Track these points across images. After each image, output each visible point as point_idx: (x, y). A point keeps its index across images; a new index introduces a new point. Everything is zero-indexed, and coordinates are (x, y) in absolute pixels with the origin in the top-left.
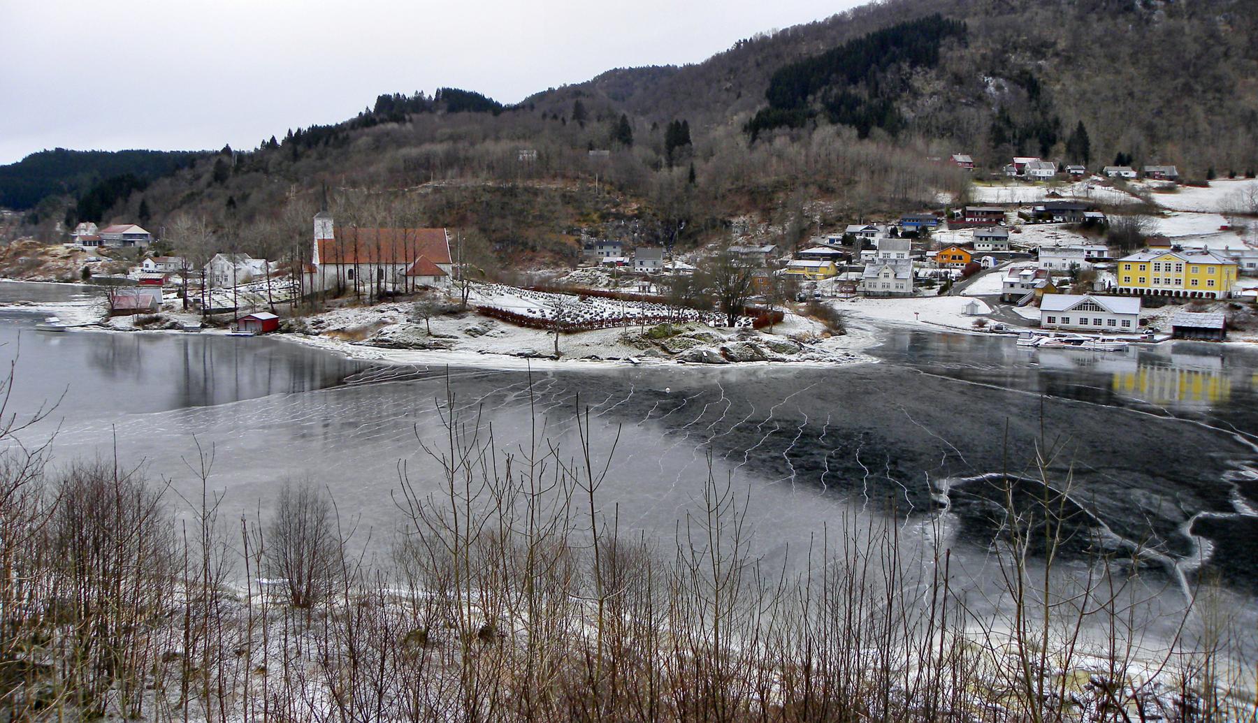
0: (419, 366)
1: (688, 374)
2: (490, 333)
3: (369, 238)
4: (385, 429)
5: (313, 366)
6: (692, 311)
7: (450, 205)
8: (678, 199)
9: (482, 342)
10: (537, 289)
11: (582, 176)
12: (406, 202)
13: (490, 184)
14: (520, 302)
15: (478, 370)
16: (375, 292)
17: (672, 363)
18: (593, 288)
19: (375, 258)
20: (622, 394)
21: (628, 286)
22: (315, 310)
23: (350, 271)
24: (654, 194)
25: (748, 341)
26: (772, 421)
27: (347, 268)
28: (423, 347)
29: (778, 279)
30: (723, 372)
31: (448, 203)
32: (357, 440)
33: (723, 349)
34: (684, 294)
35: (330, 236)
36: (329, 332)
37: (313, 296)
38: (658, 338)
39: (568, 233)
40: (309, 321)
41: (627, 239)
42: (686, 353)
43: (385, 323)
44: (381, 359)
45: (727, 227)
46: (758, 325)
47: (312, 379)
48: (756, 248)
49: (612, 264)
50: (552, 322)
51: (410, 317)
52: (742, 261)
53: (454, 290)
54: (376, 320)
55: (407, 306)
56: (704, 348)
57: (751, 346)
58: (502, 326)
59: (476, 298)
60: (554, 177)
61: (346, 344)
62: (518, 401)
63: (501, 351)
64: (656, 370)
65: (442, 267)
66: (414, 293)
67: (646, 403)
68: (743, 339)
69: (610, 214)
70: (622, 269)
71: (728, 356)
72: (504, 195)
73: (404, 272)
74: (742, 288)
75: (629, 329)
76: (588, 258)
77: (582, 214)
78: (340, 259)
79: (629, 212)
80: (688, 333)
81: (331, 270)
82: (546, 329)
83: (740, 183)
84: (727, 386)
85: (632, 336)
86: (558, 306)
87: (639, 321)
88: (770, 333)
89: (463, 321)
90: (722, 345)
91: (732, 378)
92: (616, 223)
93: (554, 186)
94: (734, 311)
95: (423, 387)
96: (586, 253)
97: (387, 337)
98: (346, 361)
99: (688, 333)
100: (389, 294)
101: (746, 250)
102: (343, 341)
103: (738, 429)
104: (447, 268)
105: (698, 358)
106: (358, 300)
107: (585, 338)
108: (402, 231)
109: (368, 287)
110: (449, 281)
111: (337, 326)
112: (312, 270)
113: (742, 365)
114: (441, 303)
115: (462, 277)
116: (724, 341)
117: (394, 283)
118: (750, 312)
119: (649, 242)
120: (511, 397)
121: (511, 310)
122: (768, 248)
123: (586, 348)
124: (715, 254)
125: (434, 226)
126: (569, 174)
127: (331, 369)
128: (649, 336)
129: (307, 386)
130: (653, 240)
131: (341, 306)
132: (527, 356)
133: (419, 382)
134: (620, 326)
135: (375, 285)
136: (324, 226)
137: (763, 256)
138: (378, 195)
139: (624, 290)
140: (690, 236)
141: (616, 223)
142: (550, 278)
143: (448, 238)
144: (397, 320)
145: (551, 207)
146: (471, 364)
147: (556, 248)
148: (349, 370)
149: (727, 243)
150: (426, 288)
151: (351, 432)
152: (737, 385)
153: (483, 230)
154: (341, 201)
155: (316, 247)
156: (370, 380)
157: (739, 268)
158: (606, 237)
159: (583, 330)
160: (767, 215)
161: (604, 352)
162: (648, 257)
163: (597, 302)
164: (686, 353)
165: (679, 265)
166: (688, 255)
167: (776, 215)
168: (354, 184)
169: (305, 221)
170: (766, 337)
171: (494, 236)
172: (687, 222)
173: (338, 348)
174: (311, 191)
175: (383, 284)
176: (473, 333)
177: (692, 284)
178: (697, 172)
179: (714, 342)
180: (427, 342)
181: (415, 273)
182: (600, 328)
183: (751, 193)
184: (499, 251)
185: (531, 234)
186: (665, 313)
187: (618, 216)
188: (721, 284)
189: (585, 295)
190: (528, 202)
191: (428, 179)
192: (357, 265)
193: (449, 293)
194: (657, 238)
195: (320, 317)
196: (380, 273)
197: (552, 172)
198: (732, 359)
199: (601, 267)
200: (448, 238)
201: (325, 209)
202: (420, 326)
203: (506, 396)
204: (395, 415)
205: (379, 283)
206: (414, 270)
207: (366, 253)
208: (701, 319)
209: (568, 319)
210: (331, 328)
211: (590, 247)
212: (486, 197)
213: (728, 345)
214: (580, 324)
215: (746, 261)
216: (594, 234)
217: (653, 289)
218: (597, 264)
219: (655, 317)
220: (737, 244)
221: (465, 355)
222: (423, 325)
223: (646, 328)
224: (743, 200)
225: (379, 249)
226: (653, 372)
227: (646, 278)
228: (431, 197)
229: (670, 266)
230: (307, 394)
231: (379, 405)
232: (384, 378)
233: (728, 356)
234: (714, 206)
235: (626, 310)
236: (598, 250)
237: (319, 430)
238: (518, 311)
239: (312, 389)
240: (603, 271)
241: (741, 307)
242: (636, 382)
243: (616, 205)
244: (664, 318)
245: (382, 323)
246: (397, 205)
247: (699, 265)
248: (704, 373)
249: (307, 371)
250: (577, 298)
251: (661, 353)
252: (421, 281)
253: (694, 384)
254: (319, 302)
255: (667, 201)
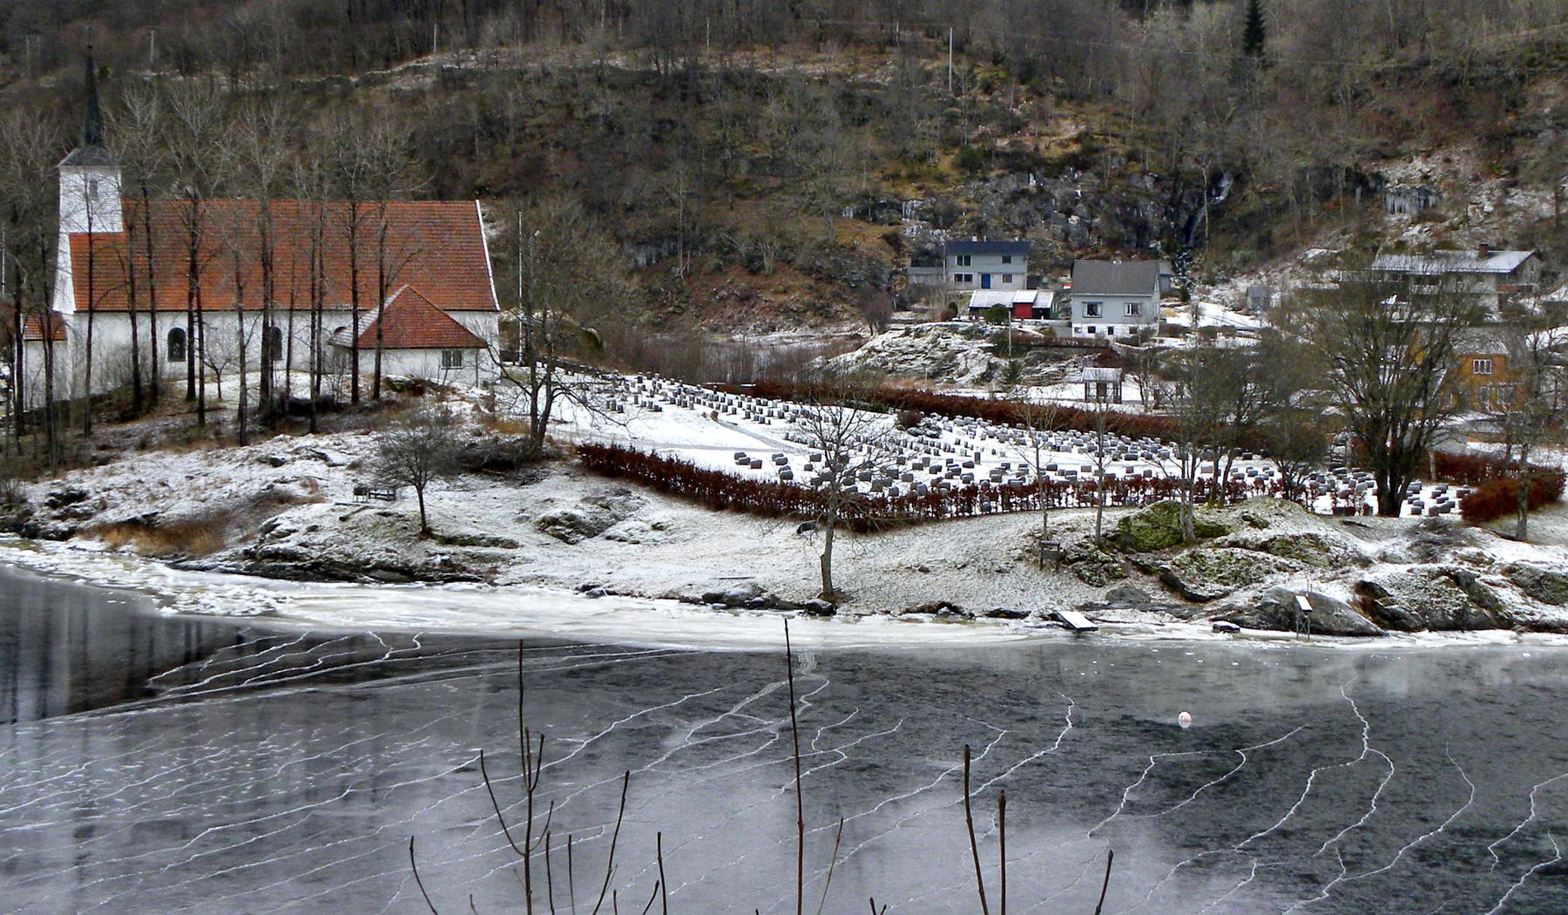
0: (391, 637)
1: (1248, 666)
2: (618, 529)
3: (236, 232)
4: (280, 842)
5: (47, 637)
6: (1258, 464)
7: (493, 128)
8: (1209, 107)
9: (592, 558)
10: (765, 391)
11: (906, 35)
12: (355, 120)
13: (619, 61)
14: (714, 433)
15: (579, 647)
16: (253, 401)
17: (1196, 631)
18: (940, 389)
19: (255, 293)
20: (1035, 730)
21: (1051, 380)
22: (55, 460)
23: (176, 336)
24: (1131, 91)
25: (1447, 561)
26: (1537, 832)
27: (166, 325)
28: (405, 574)
29: (1541, 360)
30: (1366, 663)
31: (487, 121)
32: (185, 881)
33: (1364, 587)
34: (1228, 406)
35: (111, 222)
36: (104, 530)
37: (55, 413)
38: (1150, 549)
39: (861, 215)
40: (38, 493)
41: (1043, 233)
42: (1242, 598)
43: (286, 500)
44: (270, 613)
45: (1369, 193)
46: (1477, 512)
47: (44, 682)
48: (1469, 261)
49: (998, 313)
50: (812, 496)
51: (366, 479)
52: (1420, 302)
53: (506, 393)
54: (255, 488)
55: (359, 444)
56: (1299, 584)
57: (1456, 579)
58: (657, 509)
59: (574, 421)
60: (818, 40)
61: (159, 566)
62: (709, 749)
63: (656, 584)
64: (1143, 654)
65: (470, 321)
66: (378, 405)
67: (1117, 760)
68: (1428, 556)
69: (989, 154)
70: (1029, 327)
71: (1378, 610)
72: (660, 97)
73: (347, 338)
74: (1424, 391)
75: (1056, 519)
76: (921, 292)
77: (903, 155)
78: (143, 299)
79: (1053, 151)
80: (1248, 534)
81: (114, 333)
82: (795, 517)
83: (1413, 53)
84: (1381, 712)
85: (1067, 542)
86: (834, 451)
87: (1087, 493)
88: (1520, 536)
89: (535, 492)
90: (1358, 574)
91: (1396, 685)
92: (1011, 184)
93: (815, 69)
94: (1396, 466)
95: (404, 705)
96: (918, 276)
97: (290, 544)
98: (155, 622)
99: (1248, 534)
100: (299, 407)
101: (1434, 268)
102: (147, 556)
103: (1423, 855)
104: (484, 325)
105: (1282, 616)
106: (200, 427)
107: (916, 546)
108: (343, 208)
109: (230, 385)
110: (489, 365)
111: (130, 510)
112: (51, 331)
113: (1429, 641)
114: (463, 436)
115: (530, 351)
116: (1366, 563)
117: (317, 371)
118: (1451, 469)
119: (1114, 243)
120: (683, 738)
121: (684, 456)
122: (1506, 261)
123: (919, 579)
124: (1329, 279)
125: (442, 194)
126: (864, 31)
127: (105, 649)
128: (1121, 540)
129: (27, 702)
130: (1130, 238)
131: (143, 446)
132: (731, 603)
133: (391, 687)
134: (1026, 509)
135: (254, 379)
136: (91, 194)
137: (1489, 285)
138: (264, 96)
139: (1038, 396)
140: (1247, 223)
141: (1011, 184)
142: (805, 355)
143: (486, 232)
144: (325, 484)
145: (808, 134)
146: (558, 628)
147: (826, 263)
148: (163, 650)
149: (1369, 242)
150: (416, 387)
151: (169, 851)
152: (1410, 706)
153: (596, 207)
154: (146, 112)
155: (65, 259)
156: (233, 684)
157: (1410, 326)
158: (980, 228)
159: (912, 523)
160: (1502, 154)
161: (977, 593)
162: (1113, 292)
163: (952, 433)
164: (1242, 598)
165: (1213, 314)
166: (1243, 284)
167: (1532, 155)
168: (187, 61)
169: (30, 176)
170: (1507, 552)
171: (631, 225)
172: (1239, 179)
173: (131, 579)
174: (47, 81)
175: (279, 377)
176: (566, 530)
177: (1259, 377)
178: (1270, 19)
179: (1334, 563)
180: (417, 559)
181: (381, 340)
182: (965, 514)
183: (1449, 82)
184: (648, 271)
185: (746, 221)
186: (1173, 468)
187: (1018, 162)
188: (1352, 376)
189: (916, 409)
190: (737, 118)
191: (422, 49)
192: (196, 315)
193: (490, 402)
194: (1142, 229)
195: (76, 480)
196: (272, 341)
197: (811, 24)
198: (1395, 622)
199: (964, 321)
200: (486, 232)
201: (93, 140)
202: (398, 508)
203: (667, 731)
204: (309, 795)
205: (267, 370)
206: (378, 330)
207: (226, 279)
208: (1290, 490)
209: (864, 487)
210: (111, 516)
211: (928, 258)
212: (605, 104)
213: (1379, 574)
214: (900, 503)
215: (1434, 302)
216: (942, 217)
217: (1131, 391)
218: (951, 312)
219: (1138, 483)
220: (1401, 247)
221: (539, 600)
222: (407, 503)
223: (1113, 518)
224: (1421, 107)
225: (267, 264)
226: (1138, 659)
227: (1103, 354)
228: (431, 103)
229: (1183, 319)
230: (26, 730)
231: (259, 763)
232: (279, 676)
233: (1378, 610)
234: (1325, 126)
235: (1046, 457)
236: (954, 268)
237: (63, 848)
238: (707, 461)
239: (43, 713)
240: (970, 335)
241: (1418, 450)
242: (1084, 691)
243: (1014, 127)
244: (1167, 485)
245: (275, 499)
246: (325, 125)
247: (1281, 315)
248: (1303, 666)
249: (28, 656)
250: (889, 420)
251: (1160, 596)
252: (400, 366)
253: (1269, 701)
254: (70, 434)
255: (1172, 115)
